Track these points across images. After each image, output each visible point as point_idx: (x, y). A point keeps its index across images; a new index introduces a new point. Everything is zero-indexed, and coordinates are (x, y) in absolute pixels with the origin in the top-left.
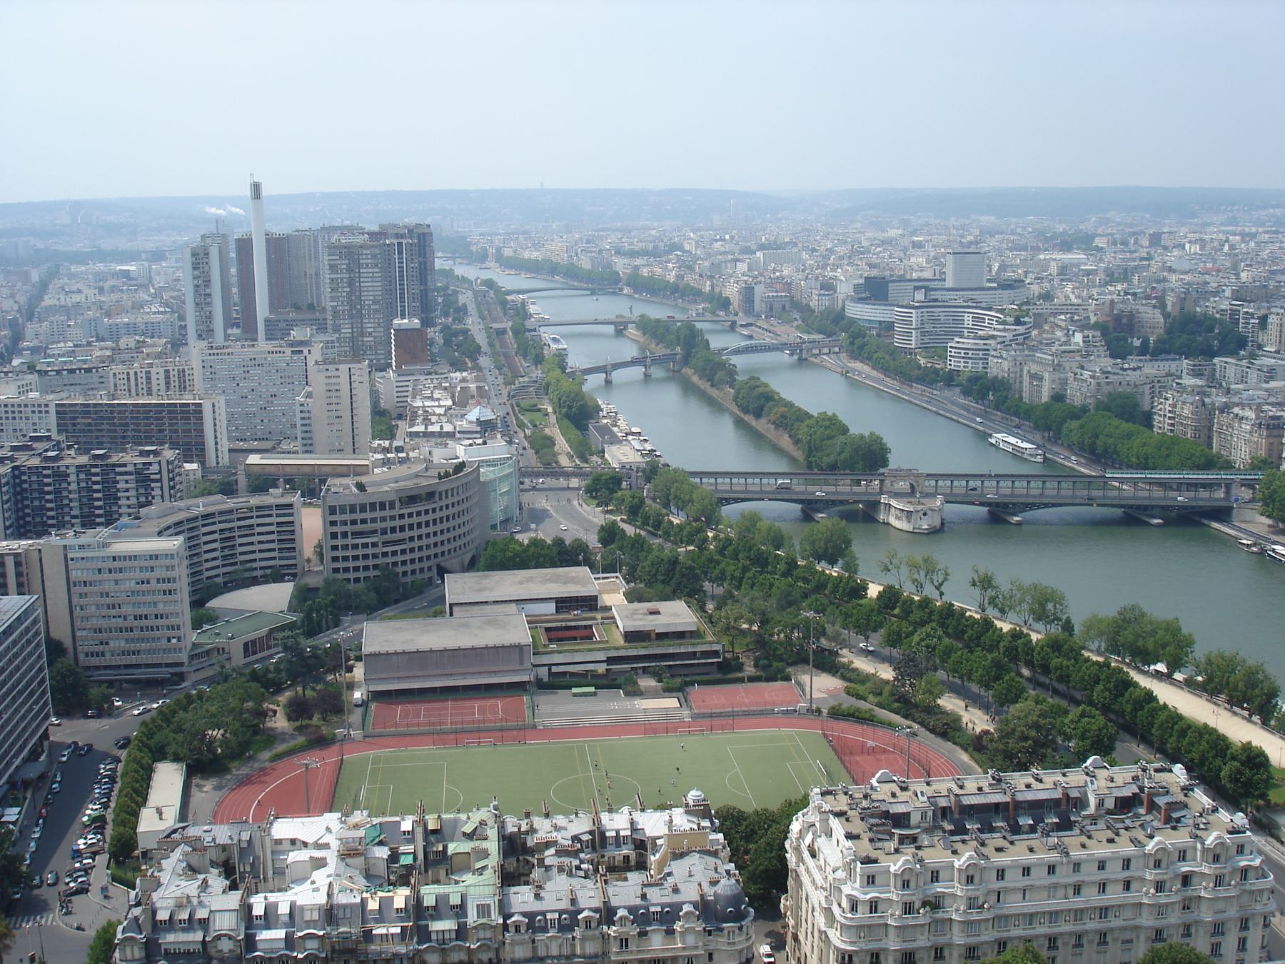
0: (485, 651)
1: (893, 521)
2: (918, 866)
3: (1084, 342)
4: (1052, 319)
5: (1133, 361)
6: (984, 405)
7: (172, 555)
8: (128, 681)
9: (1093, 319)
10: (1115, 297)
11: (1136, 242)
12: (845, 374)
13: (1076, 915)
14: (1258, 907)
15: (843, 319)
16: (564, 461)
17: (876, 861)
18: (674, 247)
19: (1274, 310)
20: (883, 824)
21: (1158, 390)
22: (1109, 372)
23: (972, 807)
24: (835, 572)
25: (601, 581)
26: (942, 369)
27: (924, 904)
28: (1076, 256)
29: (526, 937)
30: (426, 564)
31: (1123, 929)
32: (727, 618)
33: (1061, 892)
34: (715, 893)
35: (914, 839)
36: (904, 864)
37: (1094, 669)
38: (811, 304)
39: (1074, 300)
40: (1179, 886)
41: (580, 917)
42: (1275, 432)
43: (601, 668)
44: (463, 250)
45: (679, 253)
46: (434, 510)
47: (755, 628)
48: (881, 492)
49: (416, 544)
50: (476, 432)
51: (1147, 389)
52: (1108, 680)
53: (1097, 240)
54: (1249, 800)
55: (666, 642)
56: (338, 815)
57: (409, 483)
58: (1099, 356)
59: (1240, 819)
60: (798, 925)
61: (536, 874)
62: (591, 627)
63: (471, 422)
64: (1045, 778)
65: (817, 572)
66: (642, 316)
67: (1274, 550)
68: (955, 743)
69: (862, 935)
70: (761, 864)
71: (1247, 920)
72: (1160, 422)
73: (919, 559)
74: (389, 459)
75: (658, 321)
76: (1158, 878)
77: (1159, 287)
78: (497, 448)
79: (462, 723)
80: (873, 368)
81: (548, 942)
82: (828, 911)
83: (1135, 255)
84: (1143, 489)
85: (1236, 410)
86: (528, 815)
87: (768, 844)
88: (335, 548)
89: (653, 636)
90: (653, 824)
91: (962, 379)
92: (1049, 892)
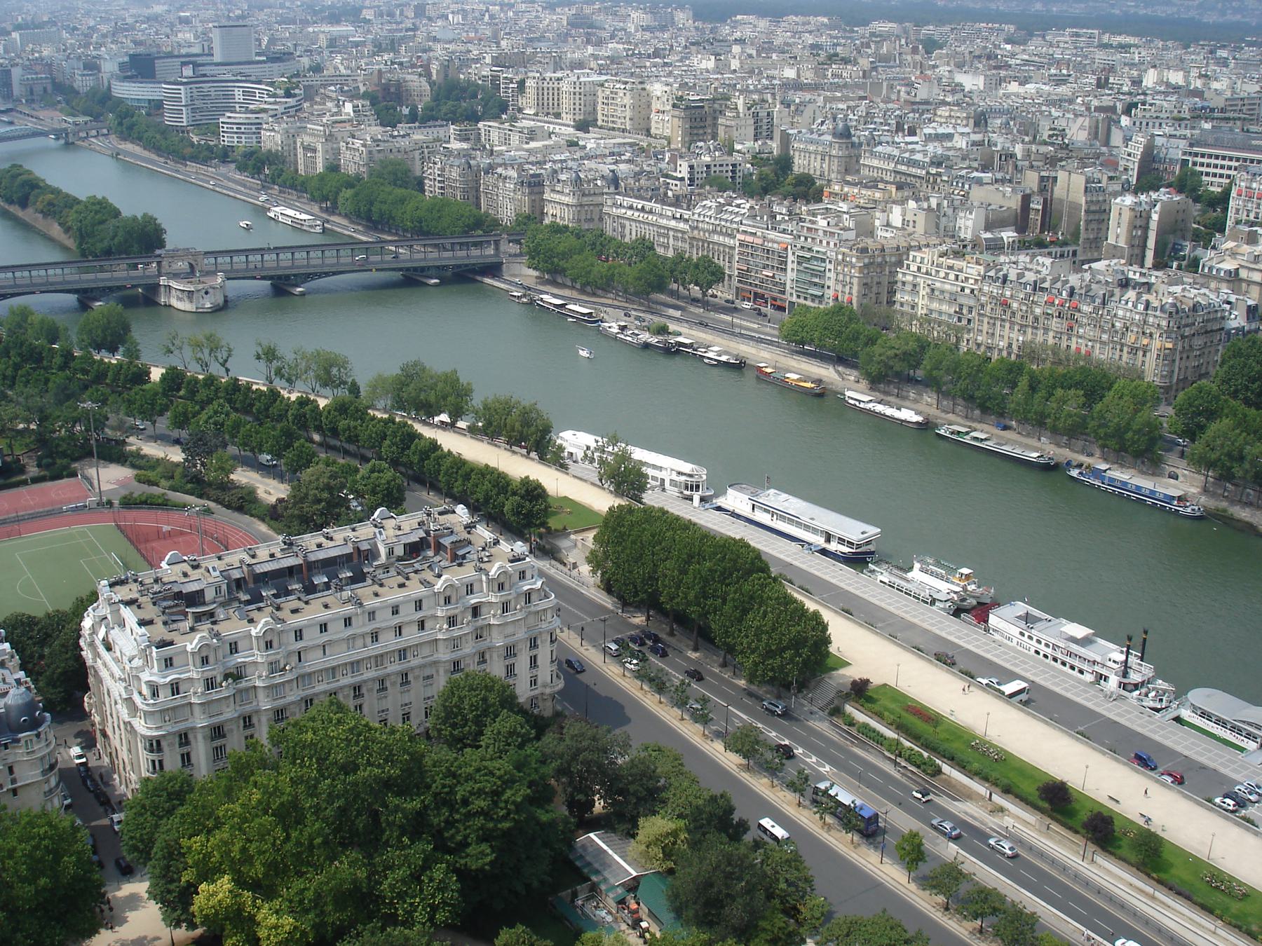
1: (175, 302)
2: (215, 641)
3: (354, 111)
4: (322, 91)
5: (402, 128)
9: (362, 89)
10: (382, 66)
11: (402, 13)
12: (116, 155)
13: (377, 662)
14: (544, 625)
15: (110, 99)
17: (171, 643)
19: (530, 74)
20: (177, 605)
21: (427, 156)
22: (380, 140)
26: (215, 146)
27: (226, 677)
28: (344, 28)
31: (422, 667)
33: (359, 642)
34: (5, 704)
35: (211, 614)
36: (200, 641)
37: (380, 426)
38: (75, 85)
39: (344, 72)
40: (470, 618)
42: (536, 189)
47: (33, 426)
48: (160, 275)
52: (394, 434)
53: (364, 12)
54: (532, 530)
58: (370, 125)
59: (520, 547)
60: (104, 721)
64: (335, 536)
65: (94, 361)
68: (252, 515)
69: (167, 718)
70: (58, 667)
73: (201, 337)
76: (449, 613)
77: (425, 56)
80: (145, 149)
82: (129, 701)
83: (400, 26)
84: (419, 252)
85: (500, 170)
87: (63, 646)
91: (237, 155)
92: (348, 644)
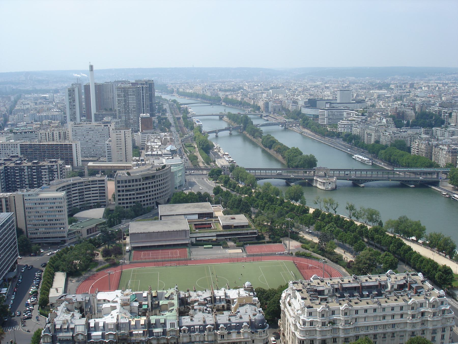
0: (173, 232)
1: (318, 186)
2: (327, 309)
3: (386, 122)
4: (375, 114)
5: (404, 129)
6: (351, 145)
7: (61, 198)
8: (46, 243)
9: (390, 114)
10: (397, 106)
11: (405, 86)
12: (301, 133)
13: (383, 327)
14: (449, 324)
15: (301, 114)
16: (201, 165)
17: (312, 307)
18: (240, 88)
19: (454, 111)
20: (315, 294)
21: (413, 139)
22: (395, 133)
23: (346, 288)
24: (297, 204)
25: (214, 207)
26: (336, 132)
27: (329, 323)
28: (383, 91)
29: (188, 334)
30: (152, 201)
31: (400, 332)
32: (259, 221)
33: (378, 318)
34: (255, 319)
35: (326, 299)
36: (322, 308)
37: (390, 239)
38: (289, 108)
39: (383, 107)
40: (420, 316)
41: (207, 327)
42: (455, 154)
43: (214, 238)
44: (165, 89)
45: (242, 90)
46: (155, 182)
47: (269, 224)
48: (314, 176)
49: (148, 194)
50: (170, 154)
51: (409, 139)
52: (395, 243)
53: (391, 86)
54: (445, 286)
55: (238, 229)
56: (121, 291)
57: (146, 173)
58: (392, 127)
59: (442, 292)
60: (284, 330)
61: (191, 312)
62: (211, 224)
63: (168, 151)
64: (372, 278)
65: (291, 204)
66: (229, 113)
67: (454, 196)
68: (340, 265)
69: (307, 334)
70: (271, 308)
71: (444, 328)
72: (413, 151)
73: (328, 199)
74: (139, 164)
75: (235, 114)
76: (413, 313)
77: (413, 102)
78: (177, 160)
79: (165, 258)
80: (311, 131)
81: (195, 336)
82: (295, 325)
83: (404, 91)
84: (407, 175)
85: (440, 146)
86: (188, 291)
87: (274, 301)
88: (119, 195)
89: (233, 227)
90: (233, 294)
91: (343, 135)
92: (374, 318)
